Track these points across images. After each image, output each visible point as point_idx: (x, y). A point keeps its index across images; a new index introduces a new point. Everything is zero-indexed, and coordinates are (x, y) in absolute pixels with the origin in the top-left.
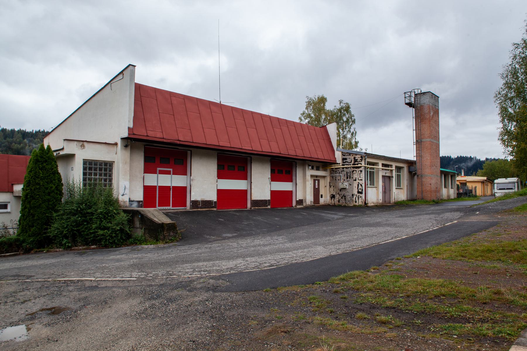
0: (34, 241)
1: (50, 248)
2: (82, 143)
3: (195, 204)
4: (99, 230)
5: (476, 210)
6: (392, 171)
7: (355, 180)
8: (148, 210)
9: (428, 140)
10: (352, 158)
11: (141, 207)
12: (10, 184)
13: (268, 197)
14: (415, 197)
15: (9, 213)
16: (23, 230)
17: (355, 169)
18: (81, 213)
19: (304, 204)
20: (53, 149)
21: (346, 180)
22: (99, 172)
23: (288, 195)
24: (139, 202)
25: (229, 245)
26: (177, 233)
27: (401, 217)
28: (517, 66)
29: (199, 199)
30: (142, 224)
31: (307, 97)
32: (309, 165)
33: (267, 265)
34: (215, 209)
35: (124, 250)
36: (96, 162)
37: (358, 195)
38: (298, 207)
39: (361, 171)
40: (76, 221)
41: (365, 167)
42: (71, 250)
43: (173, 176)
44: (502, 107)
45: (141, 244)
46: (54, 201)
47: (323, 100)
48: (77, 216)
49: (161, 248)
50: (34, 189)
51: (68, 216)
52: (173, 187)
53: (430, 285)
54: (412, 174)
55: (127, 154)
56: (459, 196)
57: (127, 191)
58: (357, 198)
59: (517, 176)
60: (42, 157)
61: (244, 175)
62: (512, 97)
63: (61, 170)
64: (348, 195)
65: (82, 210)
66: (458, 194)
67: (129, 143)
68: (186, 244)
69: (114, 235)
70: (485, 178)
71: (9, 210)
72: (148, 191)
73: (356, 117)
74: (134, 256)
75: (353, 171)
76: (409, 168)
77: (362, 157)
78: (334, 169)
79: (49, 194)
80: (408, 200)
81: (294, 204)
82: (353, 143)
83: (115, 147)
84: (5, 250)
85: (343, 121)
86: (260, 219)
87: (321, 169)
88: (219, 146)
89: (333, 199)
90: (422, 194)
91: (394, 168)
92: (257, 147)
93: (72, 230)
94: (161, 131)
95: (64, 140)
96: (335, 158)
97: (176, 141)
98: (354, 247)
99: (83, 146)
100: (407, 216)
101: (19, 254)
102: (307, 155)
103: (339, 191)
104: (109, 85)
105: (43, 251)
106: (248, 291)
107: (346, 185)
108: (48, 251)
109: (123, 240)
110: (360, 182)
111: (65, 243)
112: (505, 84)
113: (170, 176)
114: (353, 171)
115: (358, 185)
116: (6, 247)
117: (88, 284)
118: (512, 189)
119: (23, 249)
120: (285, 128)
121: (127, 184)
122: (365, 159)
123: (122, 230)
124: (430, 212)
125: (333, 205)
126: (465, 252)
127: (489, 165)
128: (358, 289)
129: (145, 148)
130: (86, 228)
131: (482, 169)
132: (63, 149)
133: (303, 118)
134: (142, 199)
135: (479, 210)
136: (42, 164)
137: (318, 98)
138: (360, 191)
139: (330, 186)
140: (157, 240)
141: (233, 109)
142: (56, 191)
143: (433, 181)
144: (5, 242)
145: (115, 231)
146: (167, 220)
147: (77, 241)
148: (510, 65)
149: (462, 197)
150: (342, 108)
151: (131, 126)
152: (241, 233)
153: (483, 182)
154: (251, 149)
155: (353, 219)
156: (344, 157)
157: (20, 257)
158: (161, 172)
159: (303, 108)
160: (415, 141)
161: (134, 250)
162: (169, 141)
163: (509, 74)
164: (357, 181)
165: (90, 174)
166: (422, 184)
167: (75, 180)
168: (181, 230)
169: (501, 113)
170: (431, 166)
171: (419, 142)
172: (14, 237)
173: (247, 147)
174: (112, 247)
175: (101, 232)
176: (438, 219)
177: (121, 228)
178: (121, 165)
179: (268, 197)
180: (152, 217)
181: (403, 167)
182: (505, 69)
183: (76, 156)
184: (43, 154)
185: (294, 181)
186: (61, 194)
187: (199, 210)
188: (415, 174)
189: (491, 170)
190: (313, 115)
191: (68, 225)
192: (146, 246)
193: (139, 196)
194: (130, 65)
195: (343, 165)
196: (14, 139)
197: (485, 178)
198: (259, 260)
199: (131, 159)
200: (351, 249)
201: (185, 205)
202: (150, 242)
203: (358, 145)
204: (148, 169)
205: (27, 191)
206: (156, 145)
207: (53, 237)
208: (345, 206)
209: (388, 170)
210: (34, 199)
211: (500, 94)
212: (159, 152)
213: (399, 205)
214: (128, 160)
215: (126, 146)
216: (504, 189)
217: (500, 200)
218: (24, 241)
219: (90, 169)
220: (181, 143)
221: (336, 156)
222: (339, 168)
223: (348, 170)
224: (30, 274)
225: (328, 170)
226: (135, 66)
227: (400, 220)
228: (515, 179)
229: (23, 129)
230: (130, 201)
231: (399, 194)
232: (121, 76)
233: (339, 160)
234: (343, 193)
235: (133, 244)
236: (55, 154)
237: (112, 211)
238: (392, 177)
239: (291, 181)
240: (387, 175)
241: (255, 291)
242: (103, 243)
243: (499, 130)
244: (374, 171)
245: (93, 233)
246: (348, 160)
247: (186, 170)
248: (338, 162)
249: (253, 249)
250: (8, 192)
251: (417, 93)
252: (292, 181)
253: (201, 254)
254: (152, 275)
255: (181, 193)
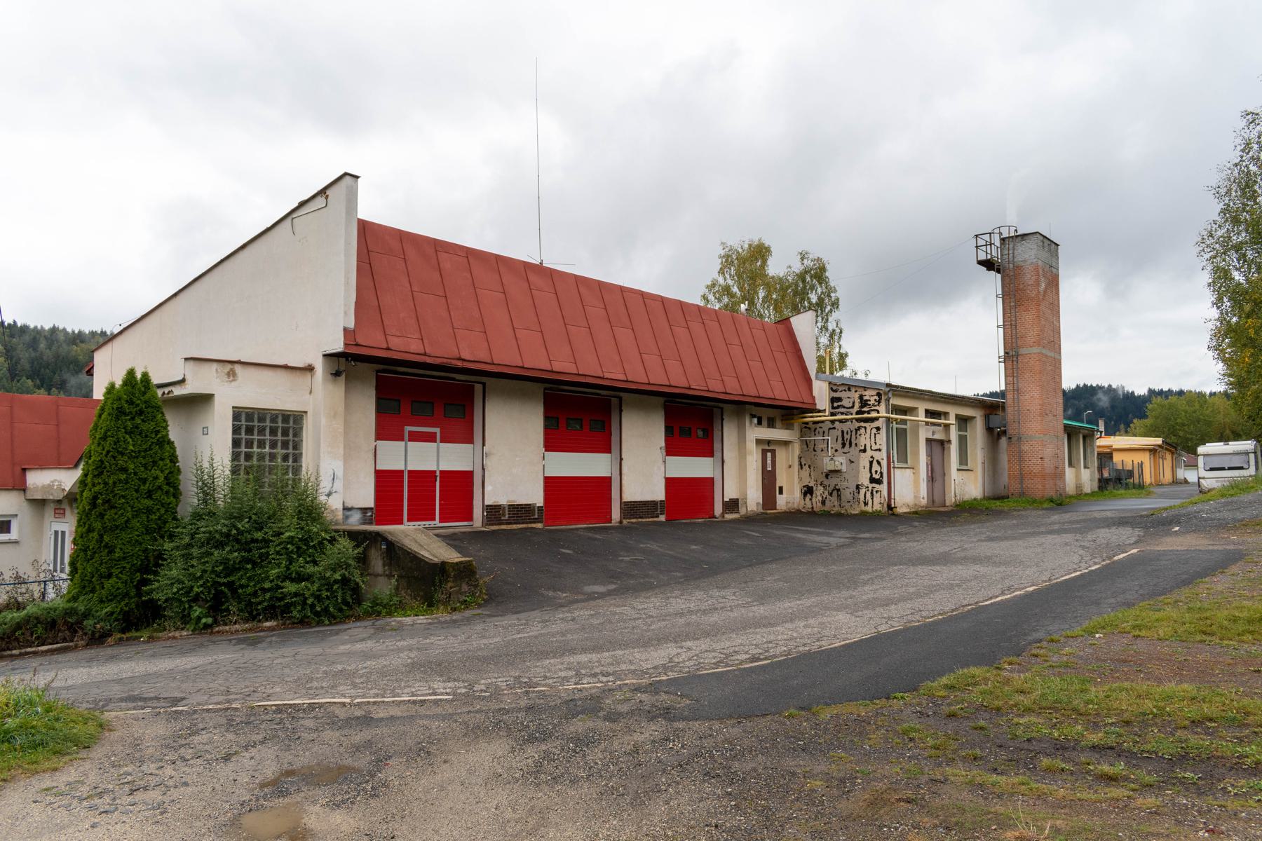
0: (112, 613)
1: (156, 630)
2: (231, 366)
3: (493, 512)
4: (287, 583)
5: (1174, 520)
6: (947, 426)
7: (864, 451)
8: (403, 532)
9: (1035, 350)
11: (371, 523)
12: (18, 470)
13: (659, 494)
14: (1002, 492)
15: (16, 542)
17: (862, 424)
18: (238, 541)
19: (743, 511)
20: (155, 380)
21: (840, 450)
22: (269, 436)
23: (600, 488)
24: (364, 510)
25: (615, 614)
26: (476, 586)
27: (991, 539)
28: (1253, 168)
29: (503, 501)
30: (390, 565)
31: (723, 243)
32: (753, 416)
33: (744, 657)
34: (539, 525)
35: (358, 629)
36: (262, 414)
37: (871, 486)
38: (729, 517)
39: (878, 429)
40: (225, 562)
41: (888, 419)
42: (212, 633)
43: (442, 445)
44: (1217, 270)
45: (390, 614)
46: (163, 511)
47: (760, 252)
48: (227, 549)
49: (446, 622)
50: (114, 483)
51: (204, 550)
52: (441, 472)
53: (1169, 698)
54: (995, 434)
55: (338, 390)
56: (1103, 484)
57: (338, 485)
58: (868, 495)
59: (1257, 438)
60: (131, 402)
61: (602, 442)
62: (1241, 243)
63: (173, 434)
64: (847, 487)
65: (240, 533)
66: (1100, 480)
67: (342, 369)
69: (325, 594)
70: (1159, 441)
71: (14, 534)
72: (386, 482)
73: (840, 294)
74: (400, 644)
75: (859, 428)
76: (987, 418)
77: (879, 395)
78: (810, 425)
79: (149, 495)
80: (985, 498)
81: (718, 509)
82: (835, 358)
83: (309, 375)
84: (38, 638)
85: (810, 303)
86: (654, 547)
87: (778, 423)
88: (552, 371)
89: (809, 496)
90: (1021, 483)
91: (952, 420)
93: (215, 583)
95: (186, 359)
96: (814, 398)
97: (454, 362)
98: (924, 614)
99: (232, 375)
100: (1006, 539)
102: (750, 391)
103: (822, 478)
104: (289, 220)
105: (137, 638)
107: (840, 462)
108: (151, 639)
110: (877, 455)
111: (199, 618)
112: (1223, 212)
113: (434, 445)
114: (859, 428)
115: (871, 463)
116: (40, 630)
118: (1241, 468)
119: (86, 634)
120: (696, 327)
122: (888, 400)
124: (1056, 527)
125: (808, 513)
126: (1209, 622)
127: (1163, 406)
128: (998, 709)
129: (378, 378)
130: (249, 579)
131: (1145, 417)
132: (183, 381)
133: (711, 297)
135: (1178, 523)
136: (133, 419)
138: (877, 477)
139: (801, 466)
140: (430, 605)
141: (579, 280)
142: (165, 488)
143: (1048, 452)
144: (37, 618)
145: (329, 585)
146: (451, 556)
147: (228, 610)
148: (1236, 165)
149: (1110, 487)
150: (806, 271)
151: (351, 324)
153: (1153, 451)
154: (622, 377)
155: (878, 545)
158: (415, 437)
160: (1002, 353)
161: (382, 629)
162: (438, 361)
163: (1234, 187)
164: (869, 453)
165: (249, 444)
166: (1020, 459)
168: (484, 579)
169: (1214, 282)
170: (1043, 414)
171: (1012, 357)
172: (61, 604)
173: (613, 373)
174: (319, 623)
175: (291, 587)
176: (1086, 544)
177: (343, 576)
178: (323, 421)
179: (659, 494)
180: (414, 547)
181: (972, 418)
182: (1223, 175)
183: (216, 398)
184: (133, 394)
185: (717, 454)
186: (177, 494)
187: (504, 527)
188: (1000, 435)
189: (1168, 419)
190: (735, 289)
191: (204, 571)
192: (408, 620)
193: (365, 496)
194: (346, 174)
195: (832, 414)
197: (1159, 441)
198: (718, 646)
200: (918, 618)
201: (469, 516)
202: (412, 608)
203: (848, 361)
204: (386, 431)
205: (96, 489)
207: (166, 601)
208: (839, 515)
209: (939, 425)
210: (113, 507)
211: (1211, 235)
212: (413, 388)
213: (967, 511)
214: (341, 408)
216: (1223, 469)
217: (1223, 496)
218: (86, 615)
219: (249, 430)
220: (466, 365)
221: (815, 393)
223: (846, 427)
225: (796, 426)
226: (357, 177)
227: (986, 549)
228: (1248, 445)
230: (346, 509)
231: (967, 484)
232: (320, 202)
233: (823, 402)
234: (833, 481)
236: (160, 392)
237: (317, 534)
238: (949, 441)
239: (608, 450)
240: (937, 437)
241: (763, 715)
242: (295, 613)
243: (1210, 325)
244: (908, 427)
245: (269, 590)
246: (846, 403)
247: (610, 434)
248: (819, 407)
250: (13, 489)
251: (1005, 235)
252: (609, 451)
253: (563, 635)
254: (483, 687)
255: (459, 487)
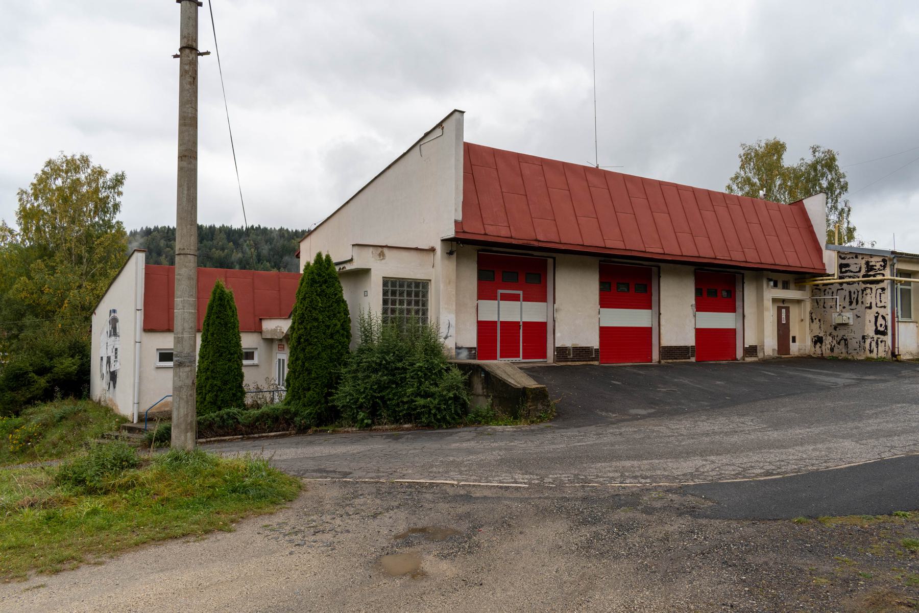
0: (311, 414)
1: (337, 426)
2: (381, 249)
3: (562, 352)
4: (418, 399)
7: (870, 308)
8: (496, 365)
10: (862, 262)
11: (475, 359)
15: (257, 366)
16: (294, 396)
17: (868, 285)
18: (387, 369)
19: (760, 355)
20: (334, 260)
21: (848, 307)
22: (406, 295)
24: (470, 349)
26: (548, 406)
29: (568, 343)
32: (771, 280)
33: (759, 471)
34: (596, 363)
37: (876, 337)
38: (748, 359)
40: (378, 382)
41: (893, 281)
45: (487, 423)
47: (777, 148)
49: (526, 431)
51: (366, 374)
52: (524, 323)
55: (451, 265)
57: (452, 331)
58: (874, 344)
60: (319, 275)
64: (854, 339)
65: (388, 363)
67: (454, 249)
68: (567, 427)
69: (443, 407)
71: (256, 361)
72: (485, 329)
75: (865, 289)
77: (884, 261)
78: (821, 287)
81: (739, 353)
85: (821, 187)
87: (792, 285)
88: (583, 245)
89: (819, 345)
92: (672, 249)
94: (506, 224)
96: (824, 265)
97: (532, 243)
99: (382, 255)
101: (290, 434)
102: (767, 259)
104: (418, 147)
105: (326, 431)
106: (763, 520)
107: (848, 316)
108: (334, 432)
109: (458, 415)
110: (882, 312)
111: (363, 420)
114: (865, 289)
115: (876, 318)
117: (451, 491)
121: (452, 318)
122: (893, 265)
123: (456, 398)
125: (818, 358)
130: (394, 394)
132: (351, 260)
134: (474, 345)
136: (321, 286)
137: (766, 144)
138: (882, 329)
139: (812, 320)
140: (516, 418)
145: (445, 400)
146: (530, 383)
147: (380, 415)
150: (817, 162)
151: (460, 218)
152: (666, 408)
154: (661, 251)
156: (844, 262)
157: (286, 440)
158: (505, 298)
159: (735, 167)
161: (482, 433)
162: (521, 242)
164: (874, 309)
165: (394, 303)
167: (373, 312)
173: (654, 248)
174: (440, 427)
175: (421, 401)
177: (455, 394)
183: (372, 271)
185: (739, 310)
186: (349, 336)
187: (569, 363)
191: (366, 388)
192: (499, 428)
193: (470, 339)
194: (455, 111)
195: (840, 278)
196: (215, 242)
199: (458, 277)
201: (544, 356)
203: (855, 234)
205: (300, 332)
206: (495, 249)
207: (343, 407)
208: (846, 360)
210: (310, 344)
214: (453, 277)
215: (450, 253)
218: (296, 414)
220: (541, 245)
221: (825, 260)
222: (832, 284)
223: (853, 288)
224: (347, 470)
229: (227, 224)
230: (457, 348)
232: (438, 132)
234: (841, 333)
235: (474, 423)
236: (337, 268)
239: (648, 306)
245: (407, 402)
246: (853, 268)
249: (707, 439)
252: (650, 307)
254: (551, 480)
255: (537, 333)
